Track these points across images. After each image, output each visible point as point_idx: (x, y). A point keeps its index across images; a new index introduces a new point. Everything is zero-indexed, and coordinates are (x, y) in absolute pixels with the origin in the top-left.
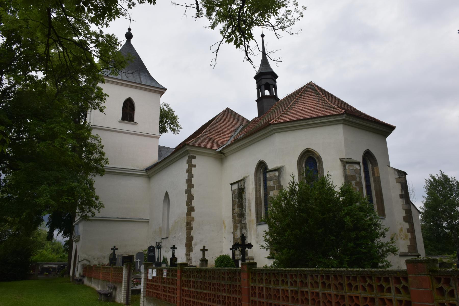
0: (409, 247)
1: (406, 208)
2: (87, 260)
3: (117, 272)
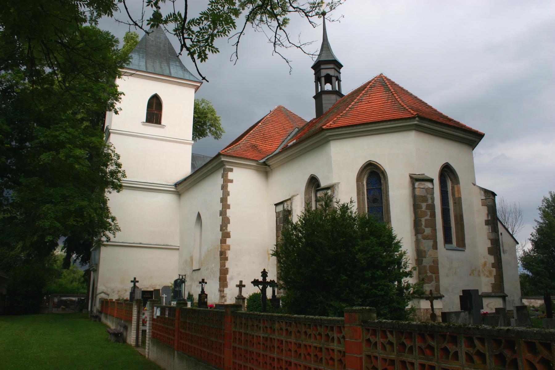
0: (494, 286)
1: (492, 238)
2: (105, 293)
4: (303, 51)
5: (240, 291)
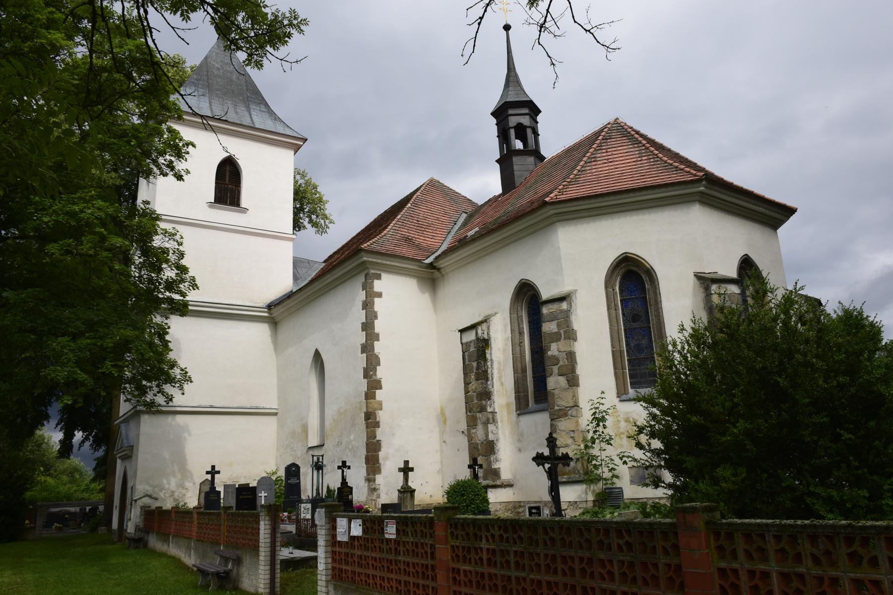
2: (150, 496)
3: (239, 524)
4: (595, 38)
5: (406, 479)
